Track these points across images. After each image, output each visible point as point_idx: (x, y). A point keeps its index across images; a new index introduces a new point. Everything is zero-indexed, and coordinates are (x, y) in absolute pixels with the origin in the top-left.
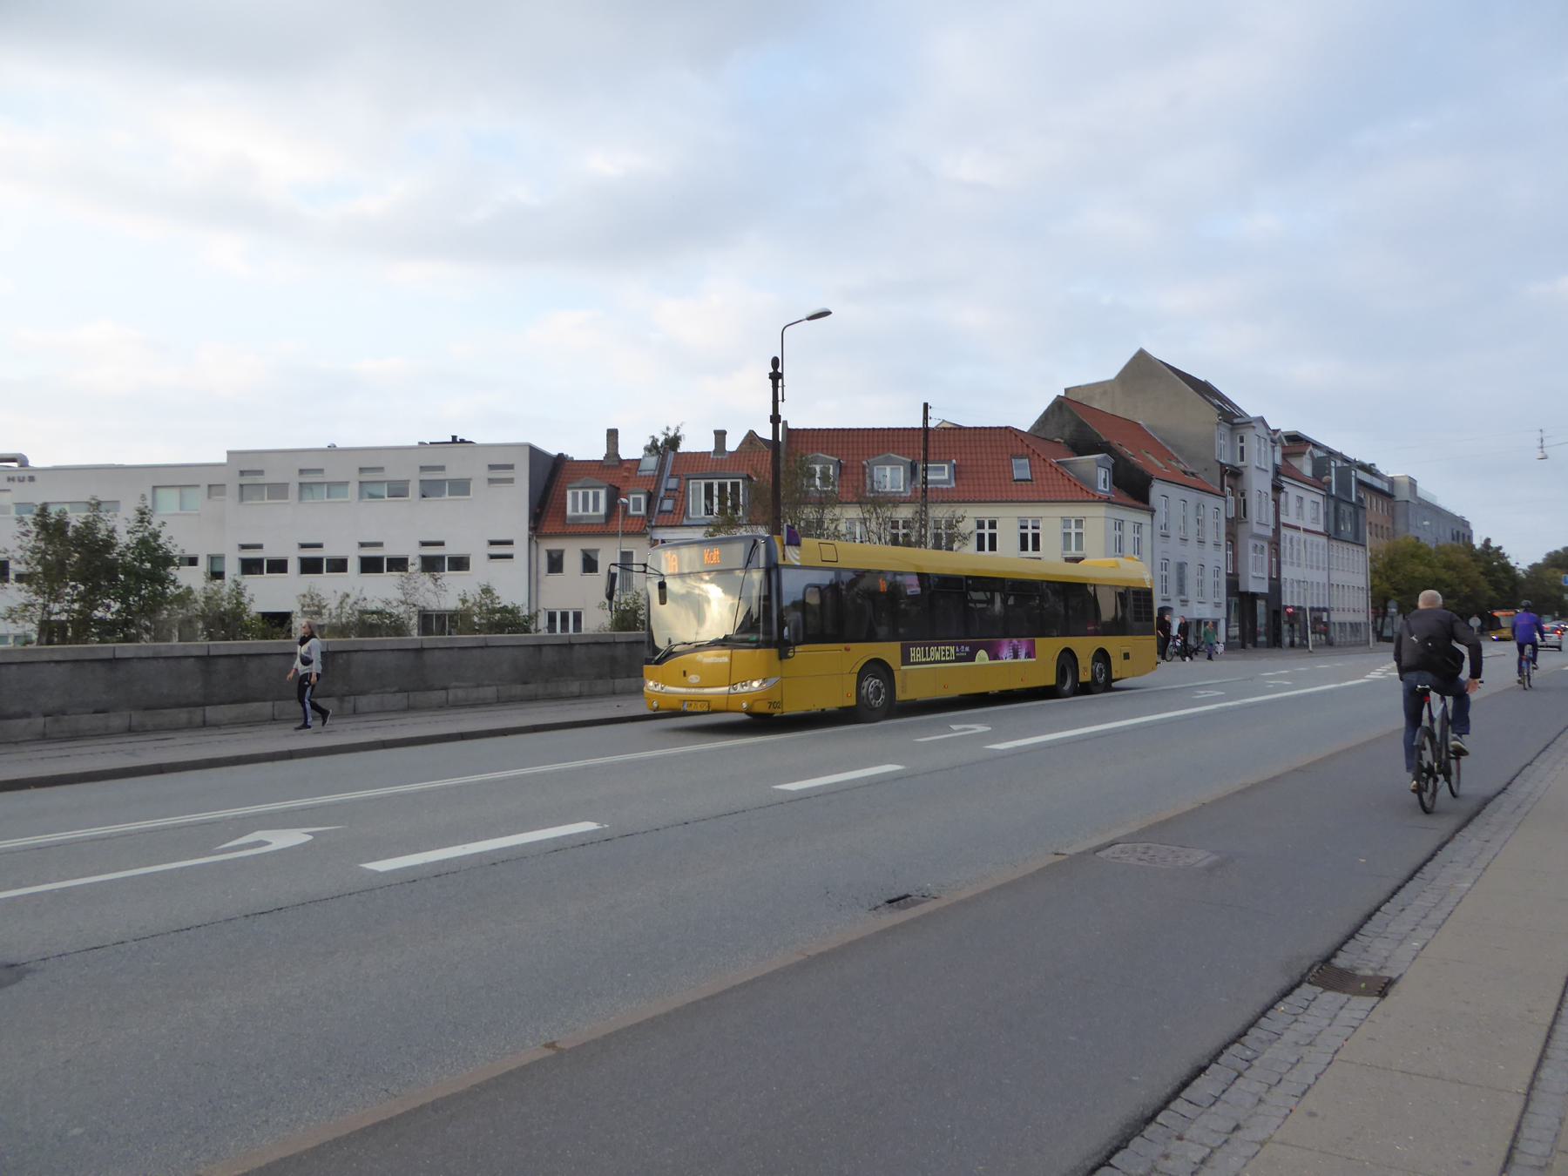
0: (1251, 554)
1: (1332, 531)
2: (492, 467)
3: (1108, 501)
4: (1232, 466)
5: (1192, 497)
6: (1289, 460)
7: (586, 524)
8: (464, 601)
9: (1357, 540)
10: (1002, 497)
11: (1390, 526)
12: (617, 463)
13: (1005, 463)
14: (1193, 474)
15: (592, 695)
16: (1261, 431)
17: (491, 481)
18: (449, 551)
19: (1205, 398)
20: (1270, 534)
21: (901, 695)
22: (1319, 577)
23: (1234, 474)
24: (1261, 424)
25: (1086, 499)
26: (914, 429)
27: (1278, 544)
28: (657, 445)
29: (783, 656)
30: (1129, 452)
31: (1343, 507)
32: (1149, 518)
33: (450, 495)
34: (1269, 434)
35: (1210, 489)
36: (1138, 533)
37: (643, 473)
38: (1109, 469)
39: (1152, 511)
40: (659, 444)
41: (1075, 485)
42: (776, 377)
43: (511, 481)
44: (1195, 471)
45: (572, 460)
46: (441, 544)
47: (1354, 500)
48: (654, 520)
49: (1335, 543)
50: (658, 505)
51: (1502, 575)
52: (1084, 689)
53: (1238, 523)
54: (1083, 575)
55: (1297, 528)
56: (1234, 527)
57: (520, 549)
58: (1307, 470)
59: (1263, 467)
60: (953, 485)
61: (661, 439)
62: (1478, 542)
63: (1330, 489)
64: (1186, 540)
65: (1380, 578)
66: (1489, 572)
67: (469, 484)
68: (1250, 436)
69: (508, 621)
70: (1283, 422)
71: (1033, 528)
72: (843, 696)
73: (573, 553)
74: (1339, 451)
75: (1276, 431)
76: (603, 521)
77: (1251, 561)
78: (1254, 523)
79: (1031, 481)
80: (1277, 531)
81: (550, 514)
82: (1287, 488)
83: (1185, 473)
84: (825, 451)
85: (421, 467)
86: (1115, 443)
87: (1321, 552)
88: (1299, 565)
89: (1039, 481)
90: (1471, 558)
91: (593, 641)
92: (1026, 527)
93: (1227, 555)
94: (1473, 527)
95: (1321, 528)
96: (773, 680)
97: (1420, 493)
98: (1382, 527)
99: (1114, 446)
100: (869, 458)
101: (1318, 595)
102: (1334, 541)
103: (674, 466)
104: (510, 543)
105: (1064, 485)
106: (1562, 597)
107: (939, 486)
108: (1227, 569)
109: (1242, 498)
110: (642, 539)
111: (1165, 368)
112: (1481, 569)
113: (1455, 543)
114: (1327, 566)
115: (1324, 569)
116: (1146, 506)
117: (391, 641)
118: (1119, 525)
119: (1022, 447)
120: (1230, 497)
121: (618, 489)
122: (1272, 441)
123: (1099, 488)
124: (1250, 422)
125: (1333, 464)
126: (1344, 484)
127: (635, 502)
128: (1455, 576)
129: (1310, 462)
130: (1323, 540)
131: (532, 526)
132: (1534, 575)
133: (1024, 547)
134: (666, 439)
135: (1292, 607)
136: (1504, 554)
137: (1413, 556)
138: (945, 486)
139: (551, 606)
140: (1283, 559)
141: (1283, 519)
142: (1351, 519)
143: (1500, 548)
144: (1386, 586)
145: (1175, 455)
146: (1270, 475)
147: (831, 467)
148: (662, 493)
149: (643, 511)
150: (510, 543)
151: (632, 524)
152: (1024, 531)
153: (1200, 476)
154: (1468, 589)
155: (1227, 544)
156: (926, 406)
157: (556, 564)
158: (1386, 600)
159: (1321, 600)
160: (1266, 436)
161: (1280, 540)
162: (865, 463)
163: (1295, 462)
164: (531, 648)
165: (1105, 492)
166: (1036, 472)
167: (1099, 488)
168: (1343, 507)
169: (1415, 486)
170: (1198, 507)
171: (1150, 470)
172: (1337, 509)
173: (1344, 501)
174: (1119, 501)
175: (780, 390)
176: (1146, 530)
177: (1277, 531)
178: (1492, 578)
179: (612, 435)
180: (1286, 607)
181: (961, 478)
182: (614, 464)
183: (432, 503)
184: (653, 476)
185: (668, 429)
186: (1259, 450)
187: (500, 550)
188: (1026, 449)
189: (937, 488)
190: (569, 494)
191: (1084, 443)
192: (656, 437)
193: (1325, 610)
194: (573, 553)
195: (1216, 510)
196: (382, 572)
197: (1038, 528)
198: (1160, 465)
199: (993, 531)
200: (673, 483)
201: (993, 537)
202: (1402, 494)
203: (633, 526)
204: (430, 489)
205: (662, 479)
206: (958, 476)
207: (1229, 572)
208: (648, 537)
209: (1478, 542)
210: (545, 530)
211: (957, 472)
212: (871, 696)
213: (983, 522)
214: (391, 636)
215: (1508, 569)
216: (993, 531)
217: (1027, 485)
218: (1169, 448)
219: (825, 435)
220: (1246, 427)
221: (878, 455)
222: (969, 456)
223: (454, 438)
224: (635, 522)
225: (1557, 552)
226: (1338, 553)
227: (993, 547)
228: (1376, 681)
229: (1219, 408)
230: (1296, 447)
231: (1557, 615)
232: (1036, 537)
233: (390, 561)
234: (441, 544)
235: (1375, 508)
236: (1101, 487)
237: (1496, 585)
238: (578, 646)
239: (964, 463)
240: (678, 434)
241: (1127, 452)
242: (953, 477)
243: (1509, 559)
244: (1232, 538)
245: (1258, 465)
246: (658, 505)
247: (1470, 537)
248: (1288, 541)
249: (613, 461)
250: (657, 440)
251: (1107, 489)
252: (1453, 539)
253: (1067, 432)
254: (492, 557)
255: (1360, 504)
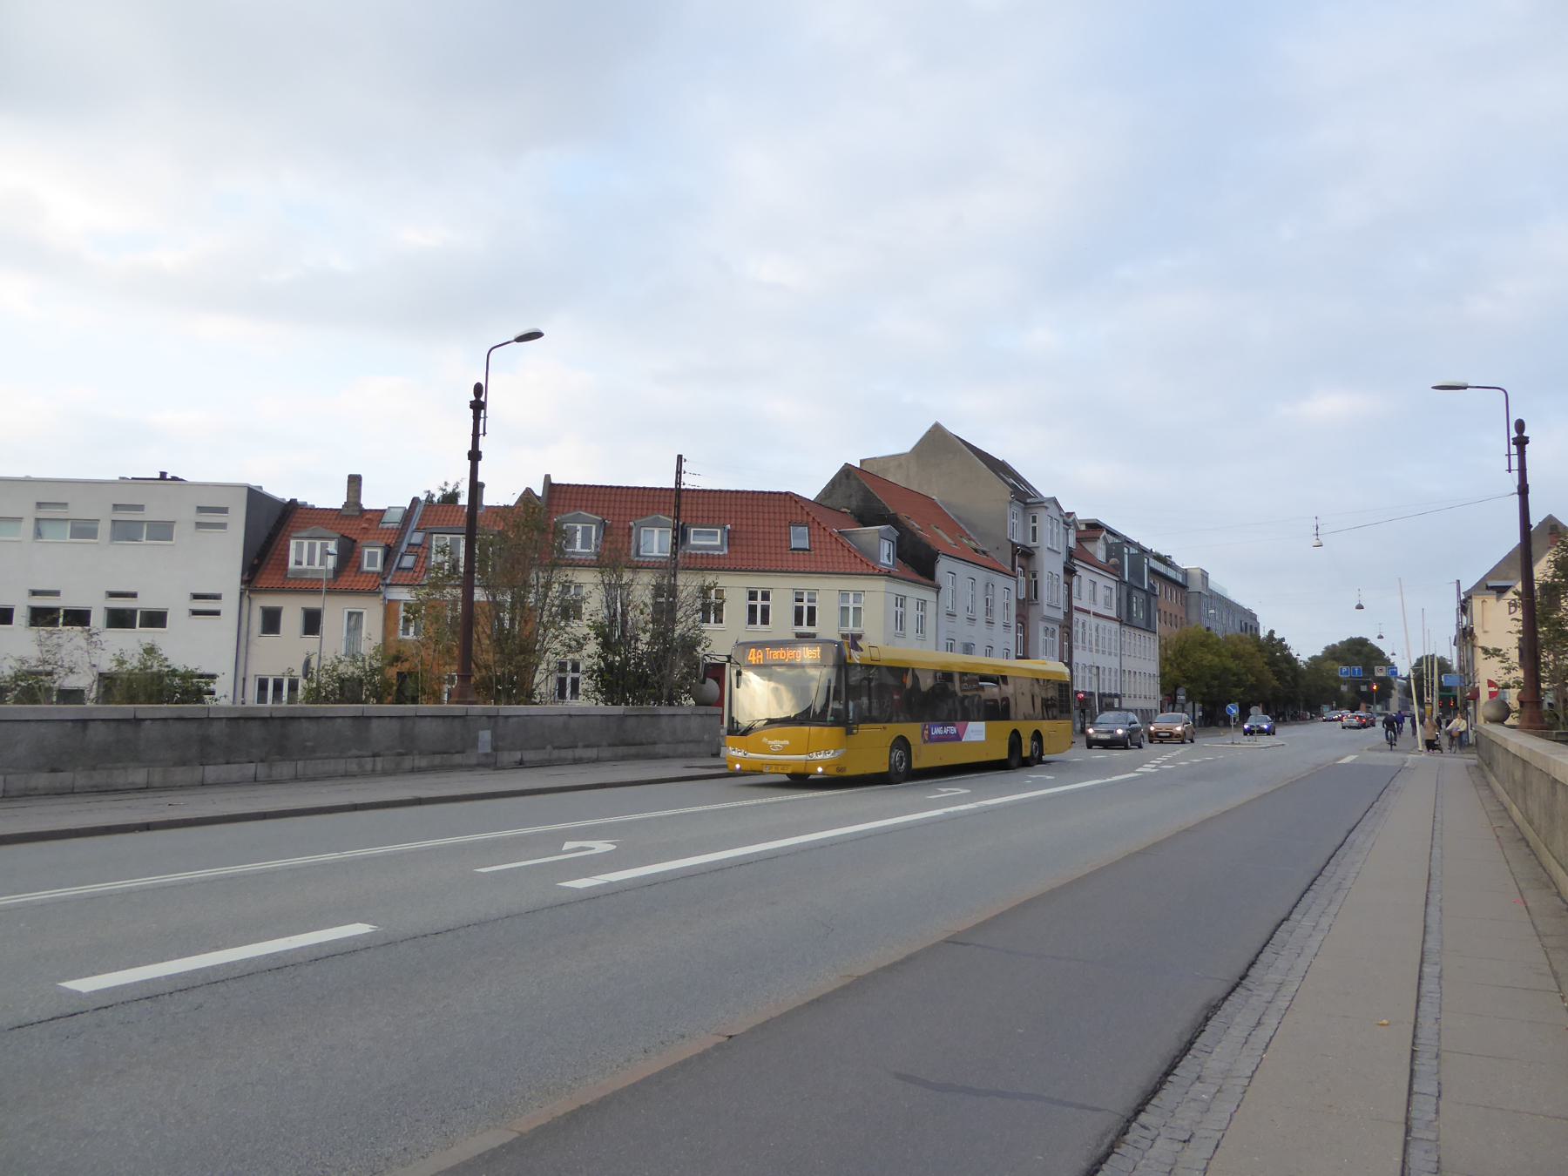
0: (1042, 636)
1: (1124, 618)
2: (201, 509)
3: (888, 574)
4: (1024, 546)
5: (981, 575)
6: (1084, 544)
7: (311, 579)
8: (121, 662)
9: (1148, 627)
10: (799, 567)
11: (1183, 616)
12: (357, 513)
13: (783, 530)
14: (984, 553)
15: (363, 774)
16: (1053, 511)
17: (199, 525)
18: (144, 603)
19: (999, 476)
20: (1061, 617)
21: (916, 765)
22: (1113, 663)
23: (1025, 554)
24: (1054, 506)
25: (865, 572)
26: (667, 489)
27: (1070, 628)
28: (432, 502)
29: (849, 732)
30: (917, 526)
31: (1135, 592)
32: (935, 595)
33: (147, 539)
34: (1061, 515)
35: (1000, 569)
36: (901, 606)
37: (386, 526)
38: (893, 542)
39: (938, 589)
40: (435, 499)
41: (855, 556)
42: (478, 406)
43: (223, 526)
44: (985, 549)
45: (312, 509)
46: (134, 595)
47: (1146, 587)
48: (390, 577)
49: (1126, 629)
50: (397, 561)
51: (1284, 666)
52: (1026, 763)
53: (1029, 604)
54: (897, 657)
55: (1088, 612)
56: (1026, 607)
57: (229, 605)
58: (1101, 555)
59: (1055, 548)
60: (726, 551)
61: (438, 495)
62: (1263, 634)
63: (1123, 575)
64: (975, 620)
65: (1171, 665)
66: (1272, 662)
67: (173, 527)
68: (1042, 515)
69: (194, 687)
70: (1083, 514)
71: (809, 601)
72: (879, 763)
73: (292, 611)
74: (1136, 541)
75: (1070, 514)
76: (331, 576)
77: (1041, 646)
78: (1045, 607)
79: (809, 550)
80: (1069, 615)
81: (269, 566)
82: (1080, 572)
83: (976, 551)
84: (589, 509)
85: (115, 505)
86: (902, 516)
87: (1113, 637)
88: (1110, 654)
89: (818, 551)
90: (1256, 649)
91: (175, 716)
92: (802, 600)
93: (1017, 637)
94: (1259, 620)
95: (1113, 614)
96: (841, 751)
97: (1211, 586)
98: (1176, 616)
99: (901, 518)
100: (636, 519)
101: (1110, 680)
102: (1127, 627)
103: (422, 519)
104: (217, 597)
105: (844, 556)
106: (1340, 688)
107: (711, 552)
108: (1017, 652)
109: (1033, 579)
110: (375, 598)
111: (959, 442)
112: (1265, 660)
113: (1243, 634)
114: (1119, 652)
115: (1116, 655)
116: (931, 582)
117: (70, 711)
118: (901, 601)
119: (802, 514)
120: (1021, 578)
121: (355, 541)
122: (1065, 523)
123: (882, 561)
124: (1043, 502)
125: (1126, 550)
126: (1136, 571)
127: (372, 558)
128: (1241, 665)
129: (1104, 547)
130: (1115, 626)
131: (246, 578)
132: (1313, 666)
133: (752, 620)
134: (444, 496)
135: (1083, 692)
136: (1286, 645)
137: (1202, 644)
138: (717, 553)
139: (263, 673)
140: (1074, 643)
141: (1076, 603)
142: (1143, 607)
143: (1283, 639)
144: (1176, 673)
145: (968, 532)
146: (1063, 557)
147: (594, 527)
148: (404, 548)
149: (378, 567)
150: (217, 597)
151: (364, 581)
152: (799, 604)
153: (991, 554)
154: (1254, 679)
155: (1017, 626)
156: (680, 457)
157: (271, 622)
158: (1177, 687)
159: (1113, 687)
160: (1059, 518)
161: (1072, 624)
162: (632, 524)
163: (1089, 547)
164: (70, 724)
165: (887, 565)
166: (814, 542)
167: (882, 561)
168: (1135, 592)
169: (1207, 578)
170: (987, 586)
171: (936, 546)
172: (1129, 596)
173: (1136, 587)
174: (901, 575)
175: (482, 421)
176: (931, 608)
177: (1069, 615)
178: (1276, 668)
179: (355, 482)
180: (1077, 693)
181: (734, 545)
182: (354, 514)
183: (127, 549)
184: (397, 529)
185: (446, 484)
186: (1052, 531)
187: (204, 605)
188: (805, 516)
189: (708, 554)
190: (293, 544)
191: (870, 514)
192: (432, 492)
193: (1116, 696)
194: (292, 611)
195: (1006, 591)
196: (134, 627)
197: (814, 601)
198: (949, 541)
199: (765, 603)
200: (417, 538)
201: (765, 611)
202: (1194, 586)
203: (365, 584)
204: (125, 531)
205: (405, 534)
206: (731, 542)
207: (1430, 707)
208: (381, 597)
209: (1263, 634)
210: (262, 583)
211: (731, 538)
212: (897, 764)
213: (756, 593)
214: (24, 704)
215: (1290, 660)
216: (765, 603)
217: (804, 554)
218: (962, 525)
219: (575, 491)
220: (1038, 507)
221: (647, 515)
222: (744, 522)
223: (163, 475)
224: (368, 579)
225: (1334, 646)
226: (1145, 643)
227: (765, 621)
228: (1146, 775)
229: (1012, 486)
230: (1092, 533)
231: (1334, 705)
232: (812, 611)
233: (68, 613)
234: (134, 595)
235: (1168, 600)
236: (884, 560)
237: (1279, 675)
238: (148, 722)
239: (738, 528)
240: (457, 490)
241: (915, 525)
242: (726, 543)
243: (1291, 651)
244: (1023, 619)
245: (1050, 546)
246: (397, 561)
247: (1257, 629)
248: (1080, 625)
249: (353, 511)
250: (433, 495)
251: (891, 563)
252: (1242, 630)
253: (854, 503)
254: (195, 613)
255: (1152, 591)
